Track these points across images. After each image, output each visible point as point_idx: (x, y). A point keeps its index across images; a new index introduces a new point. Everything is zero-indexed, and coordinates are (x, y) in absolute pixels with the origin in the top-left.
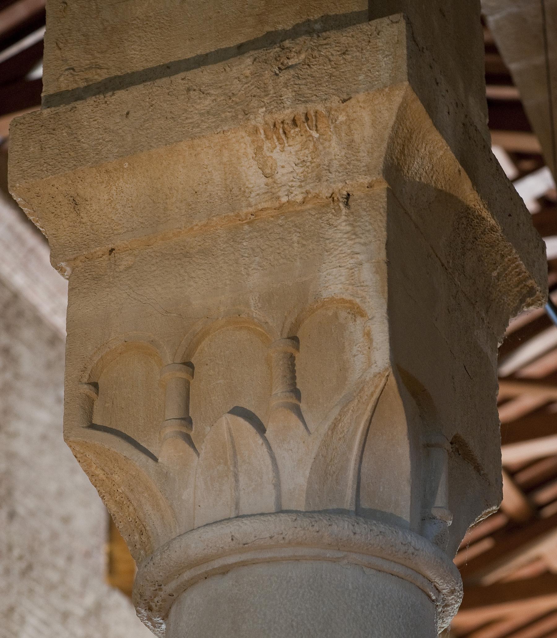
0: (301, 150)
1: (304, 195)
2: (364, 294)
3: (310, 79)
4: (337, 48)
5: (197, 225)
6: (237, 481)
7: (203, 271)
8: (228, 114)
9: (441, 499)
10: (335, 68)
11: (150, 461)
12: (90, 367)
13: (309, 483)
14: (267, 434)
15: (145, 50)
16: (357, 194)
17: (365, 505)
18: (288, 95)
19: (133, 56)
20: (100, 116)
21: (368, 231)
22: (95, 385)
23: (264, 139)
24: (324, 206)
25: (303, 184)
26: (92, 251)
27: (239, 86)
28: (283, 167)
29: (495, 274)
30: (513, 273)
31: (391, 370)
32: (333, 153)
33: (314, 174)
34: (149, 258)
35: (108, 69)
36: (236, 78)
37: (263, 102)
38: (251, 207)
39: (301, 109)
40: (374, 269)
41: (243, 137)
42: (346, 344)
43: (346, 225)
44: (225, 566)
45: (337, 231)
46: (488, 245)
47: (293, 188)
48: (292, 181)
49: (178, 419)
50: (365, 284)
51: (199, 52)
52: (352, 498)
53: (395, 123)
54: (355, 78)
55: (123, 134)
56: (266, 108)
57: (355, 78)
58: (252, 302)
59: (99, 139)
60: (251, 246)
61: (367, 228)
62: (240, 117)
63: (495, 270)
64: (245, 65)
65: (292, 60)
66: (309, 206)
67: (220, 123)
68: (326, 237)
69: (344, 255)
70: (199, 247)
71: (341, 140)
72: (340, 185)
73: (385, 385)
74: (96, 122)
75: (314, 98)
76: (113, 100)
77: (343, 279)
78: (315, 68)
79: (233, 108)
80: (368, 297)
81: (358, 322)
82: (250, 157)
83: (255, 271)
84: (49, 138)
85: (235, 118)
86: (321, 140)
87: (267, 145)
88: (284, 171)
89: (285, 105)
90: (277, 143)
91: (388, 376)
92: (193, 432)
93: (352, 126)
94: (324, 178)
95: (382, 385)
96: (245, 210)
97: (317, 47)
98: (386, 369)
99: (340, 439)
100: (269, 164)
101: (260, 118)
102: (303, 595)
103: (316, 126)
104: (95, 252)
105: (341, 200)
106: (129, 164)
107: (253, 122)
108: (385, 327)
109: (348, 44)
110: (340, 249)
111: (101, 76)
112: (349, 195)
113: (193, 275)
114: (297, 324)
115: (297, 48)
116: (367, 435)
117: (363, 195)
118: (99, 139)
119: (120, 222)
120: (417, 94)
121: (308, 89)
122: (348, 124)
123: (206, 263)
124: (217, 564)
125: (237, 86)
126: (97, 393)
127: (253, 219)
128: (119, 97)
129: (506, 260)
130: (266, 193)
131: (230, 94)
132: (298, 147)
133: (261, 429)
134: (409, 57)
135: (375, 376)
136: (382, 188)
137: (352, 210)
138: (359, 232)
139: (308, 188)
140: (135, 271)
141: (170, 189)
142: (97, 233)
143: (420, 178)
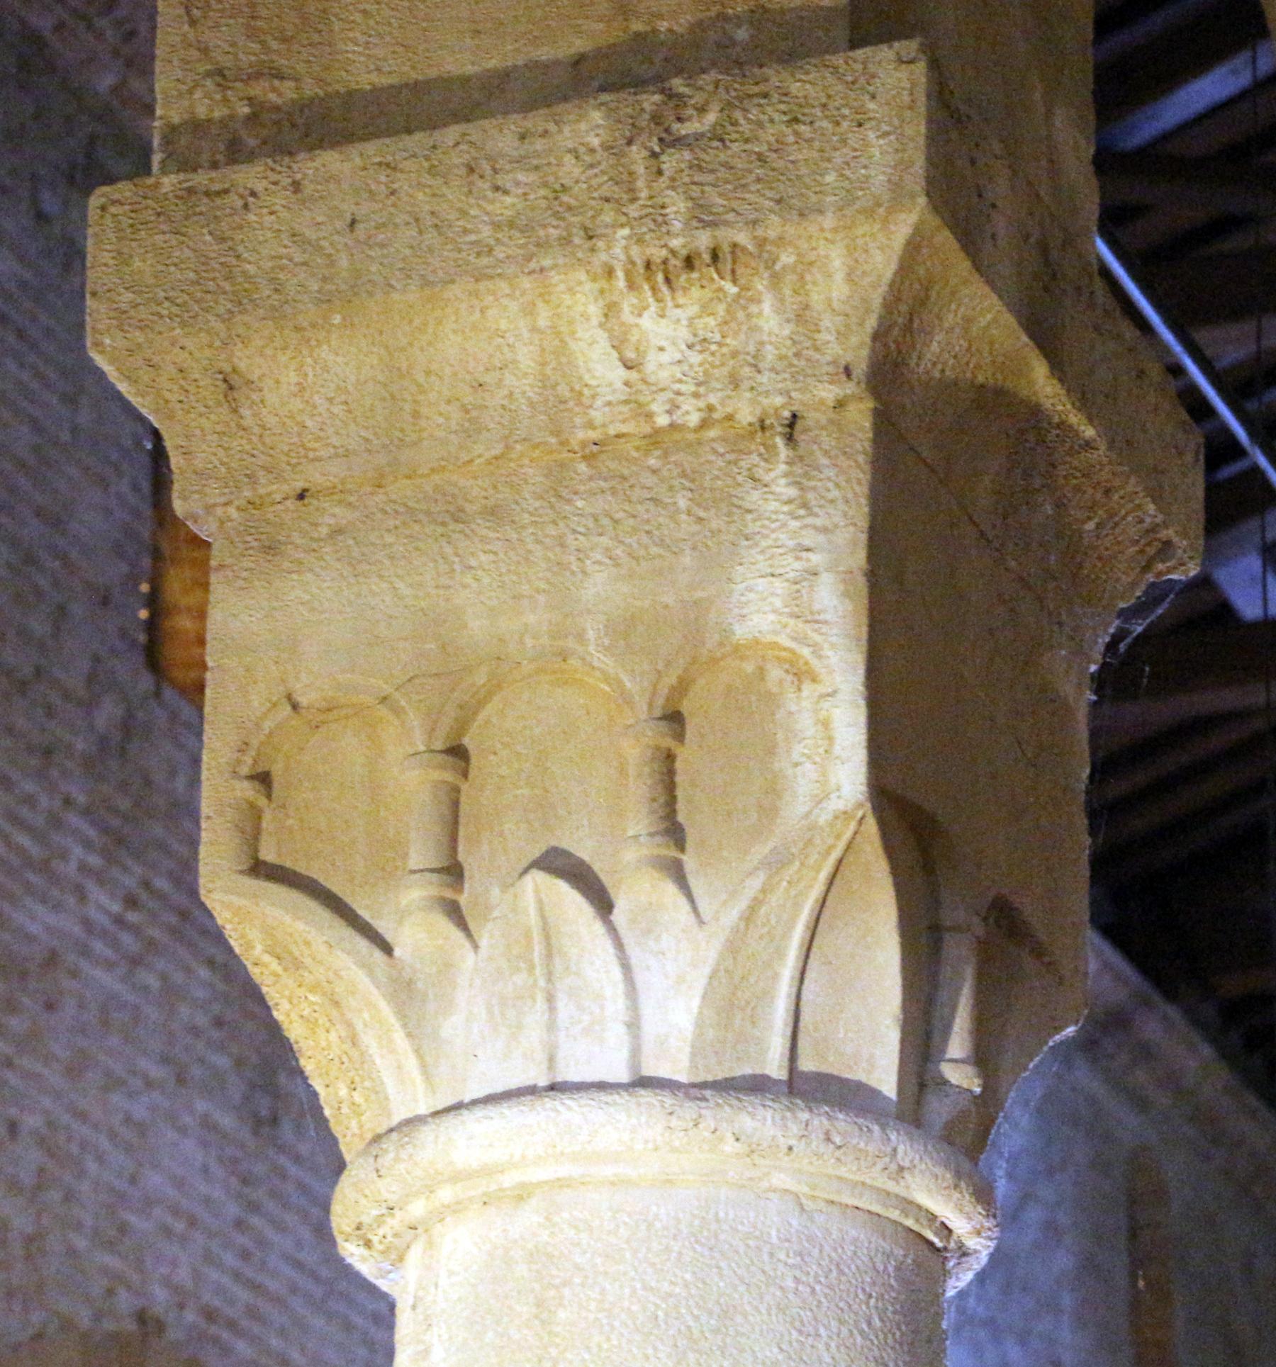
0: (700, 317)
1: (702, 414)
2: (818, 638)
3: (723, 173)
4: (782, 107)
5: (480, 456)
6: (552, 1008)
7: (492, 557)
8: (551, 230)
9: (958, 1044)
10: (775, 151)
11: (378, 955)
12: (255, 742)
13: (700, 1024)
14: (618, 916)
15: (376, 45)
16: (812, 418)
17: (807, 1064)
18: (677, 206)
19: (350, 55)
20: (283, 202)
21: (832, 501)
22: (263, 779)
23: (625, 290)
24: (743, 437)
25: (702, 390)
26: (262, 491)
27: (577, 171)
28: (661, 349)
29: (1090, 526)
30: (1130, 519)
31: (869, 805)
32: (766, 328)
33: (725, 370)
34: (379, 515)
35: (297, 80)
36: (569, 151)
37: (624, 214)
38: (594, 428)
39: (704, 240)
40: (842, 587)
41: (580, 283)
42: (780, 736)
43: (789, 484)
44: (523, 1185)
45: (770, 497)
46: (1078, 474)
47: (681, 398)
48: (680, 381)
49: (432, 871)
50: (822, 617)
51: (492, 64)
52: (782, 1055)
53: (896, 274)
54: (818, 178)
55: (330, 251)
56: (632, 229)
57: (818, 178)
58: (591, 634)
59: (281, 258)
60: (592, 511)
61: (830, 496)
62: (577, 241)
63: (1089, 518)
64: (590, 125)
65: (688, 124)
66: (712, 433)
67: (534, 249)
68: (748, 506)
69: (780, 551)
70: (483, 501)
71: (782, 300)
72: (779, 400)
73: (856, 833)
74: (273, 217)
75: (730, 217)
76: (311, 172)
77: (778, 603)
78: (735, 147)
79: (563, 219)
80: (826, 646)
81: (805, 693)
82: (595, 321)
83: (597, 567)
84: (174, 243)
85: (566, 241)
86: (742, 301)
87: (628, 305)
88: (665, 358)
89: (672, 229)
90: (651, 300)
91: (862, 818)
92: (466, 895)
93: (808, 277)
94: (746, 384)
95: (848, 834)
96: (581, 435)
97: (741, 100)
98: (860, 805)
99: (761, 938)
100: (634, 339)
101: (619, 246)
102: (680, 1254)
103: (733, 271)
104: (269, 494)
105: (780, 429)
106: (344, 319)
107: (603, 257)
108: (859, 715)
109: (805, 97)
110: (773, 536)
111: (280, 95)
112: (794, 416)
113: (473, 563)
114: (682, 688)
115: (698, 98)
116: (816, 927)
117: (824, 421)
118: (281, 258)
119: (322, 434)
120: (943, 218)
121: (720, 195)
122: (799, 270)
123: (498, 539)
124: (509, 1180)
125: (570, 169)
126: (269, 797)
127: (595, 451)
128: (324, 166)
129: (1116, 497)
130: (626, 402)
131: (557, 187)
132: (695, 309)
133: (602, 902)
134: (931, 139)
135: (836, 818)
136: (861, 415)
137: (801, 452)
138: (814, 503)
139: (713, 399)
140: (351, 542)
141: (428, 373)
142: (271, 452)
143: (943, 371)
